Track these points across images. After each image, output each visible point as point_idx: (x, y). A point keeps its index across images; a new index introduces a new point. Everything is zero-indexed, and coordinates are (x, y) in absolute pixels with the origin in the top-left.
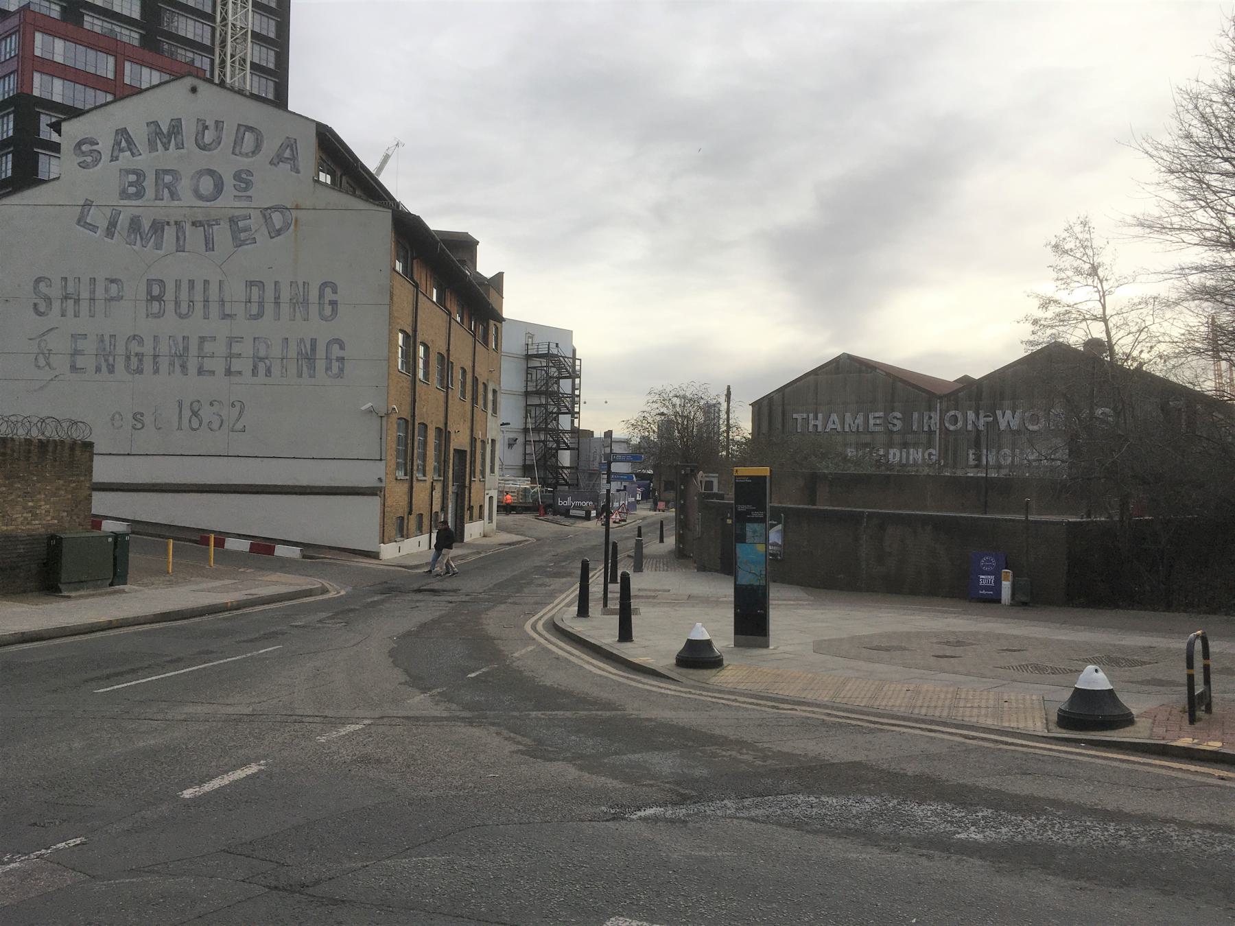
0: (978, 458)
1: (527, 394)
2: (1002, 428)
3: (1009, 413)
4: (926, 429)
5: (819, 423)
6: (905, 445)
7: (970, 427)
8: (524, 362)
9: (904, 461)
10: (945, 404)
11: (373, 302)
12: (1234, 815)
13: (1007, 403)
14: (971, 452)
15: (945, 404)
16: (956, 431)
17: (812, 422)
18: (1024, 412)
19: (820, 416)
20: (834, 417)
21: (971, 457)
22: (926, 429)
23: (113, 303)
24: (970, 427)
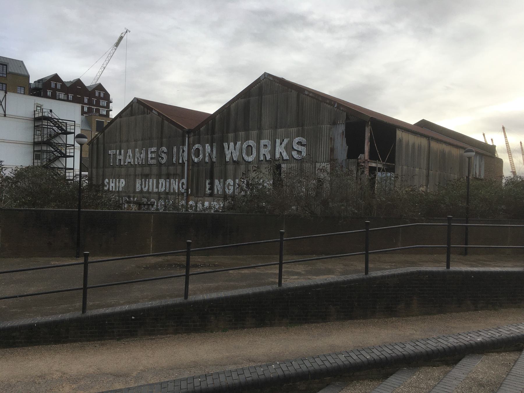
0: (212, 188)
1: (35, 144)
2: (228, 159)
3: (232, 144)
4: (181, 162)
5: (122, 157)
6: (168, 176)
7: (207, 159)
8: (33, 122)
9: (167, 190)
10: (191, 139)
11: (132, 114)
12: (523, 382)
13: (231, 135)
14: (208, 182)
15: (191, 139)
16: (198, 163)
17: (118, 157)
18: (242, 144)
19: (122, 151)
20: (130, 151)
21: (208, 186)
22: (181, 162)
23: (6, 113)
24: (207, 159)
